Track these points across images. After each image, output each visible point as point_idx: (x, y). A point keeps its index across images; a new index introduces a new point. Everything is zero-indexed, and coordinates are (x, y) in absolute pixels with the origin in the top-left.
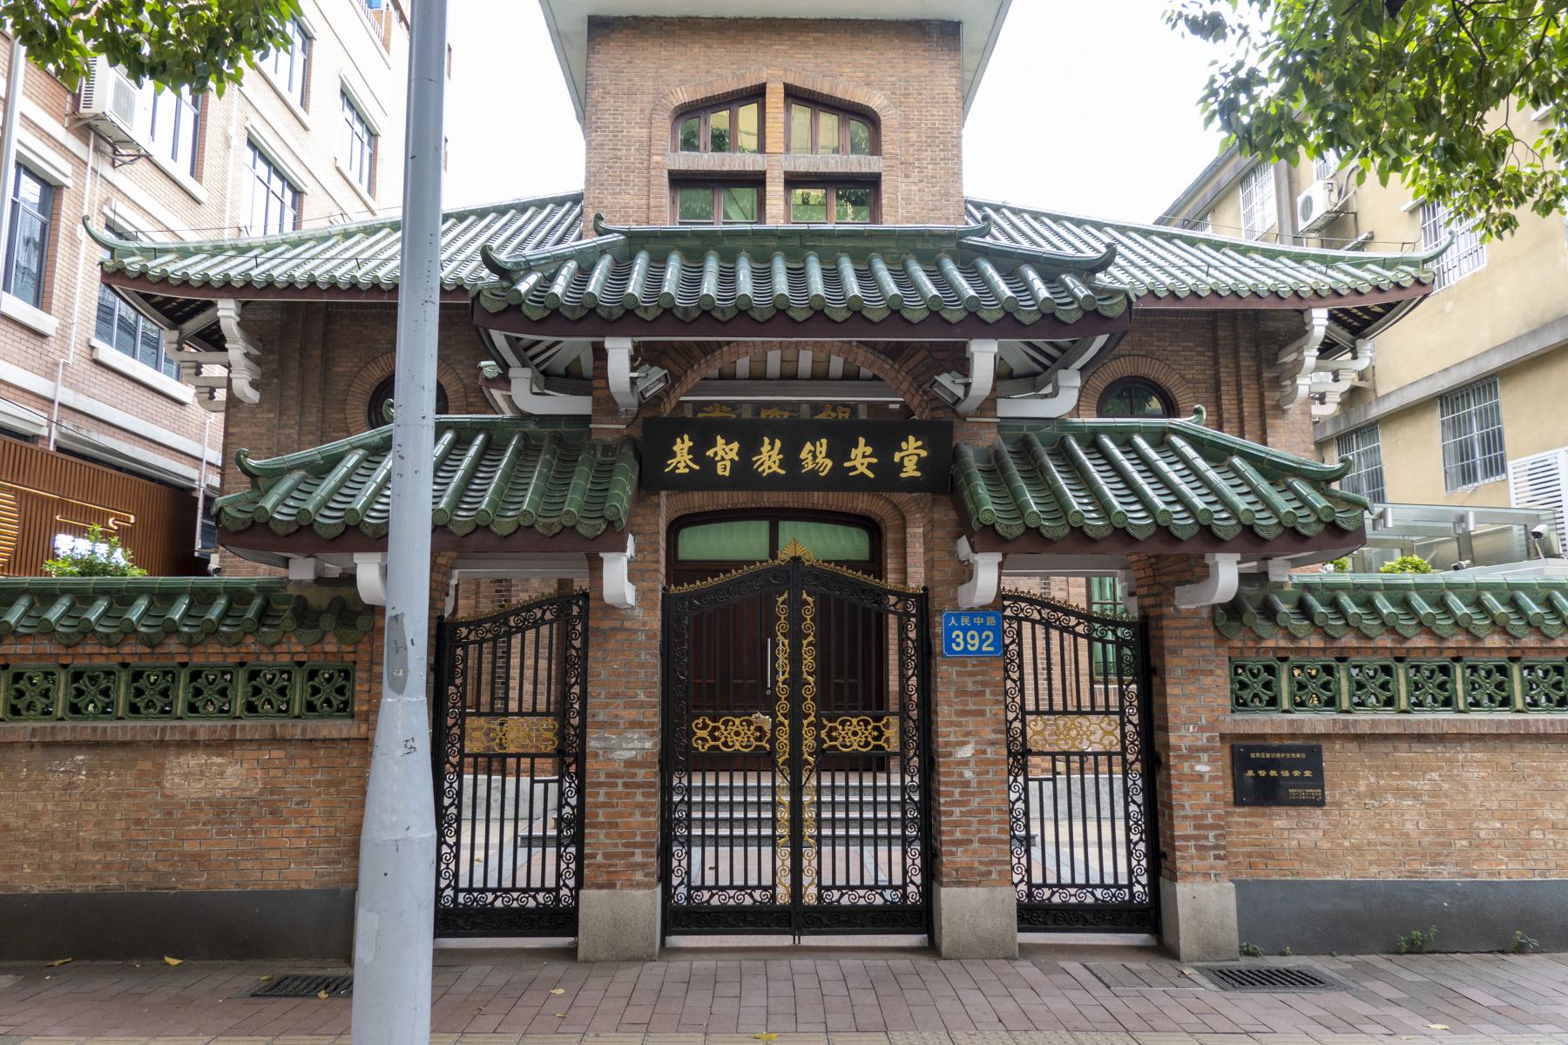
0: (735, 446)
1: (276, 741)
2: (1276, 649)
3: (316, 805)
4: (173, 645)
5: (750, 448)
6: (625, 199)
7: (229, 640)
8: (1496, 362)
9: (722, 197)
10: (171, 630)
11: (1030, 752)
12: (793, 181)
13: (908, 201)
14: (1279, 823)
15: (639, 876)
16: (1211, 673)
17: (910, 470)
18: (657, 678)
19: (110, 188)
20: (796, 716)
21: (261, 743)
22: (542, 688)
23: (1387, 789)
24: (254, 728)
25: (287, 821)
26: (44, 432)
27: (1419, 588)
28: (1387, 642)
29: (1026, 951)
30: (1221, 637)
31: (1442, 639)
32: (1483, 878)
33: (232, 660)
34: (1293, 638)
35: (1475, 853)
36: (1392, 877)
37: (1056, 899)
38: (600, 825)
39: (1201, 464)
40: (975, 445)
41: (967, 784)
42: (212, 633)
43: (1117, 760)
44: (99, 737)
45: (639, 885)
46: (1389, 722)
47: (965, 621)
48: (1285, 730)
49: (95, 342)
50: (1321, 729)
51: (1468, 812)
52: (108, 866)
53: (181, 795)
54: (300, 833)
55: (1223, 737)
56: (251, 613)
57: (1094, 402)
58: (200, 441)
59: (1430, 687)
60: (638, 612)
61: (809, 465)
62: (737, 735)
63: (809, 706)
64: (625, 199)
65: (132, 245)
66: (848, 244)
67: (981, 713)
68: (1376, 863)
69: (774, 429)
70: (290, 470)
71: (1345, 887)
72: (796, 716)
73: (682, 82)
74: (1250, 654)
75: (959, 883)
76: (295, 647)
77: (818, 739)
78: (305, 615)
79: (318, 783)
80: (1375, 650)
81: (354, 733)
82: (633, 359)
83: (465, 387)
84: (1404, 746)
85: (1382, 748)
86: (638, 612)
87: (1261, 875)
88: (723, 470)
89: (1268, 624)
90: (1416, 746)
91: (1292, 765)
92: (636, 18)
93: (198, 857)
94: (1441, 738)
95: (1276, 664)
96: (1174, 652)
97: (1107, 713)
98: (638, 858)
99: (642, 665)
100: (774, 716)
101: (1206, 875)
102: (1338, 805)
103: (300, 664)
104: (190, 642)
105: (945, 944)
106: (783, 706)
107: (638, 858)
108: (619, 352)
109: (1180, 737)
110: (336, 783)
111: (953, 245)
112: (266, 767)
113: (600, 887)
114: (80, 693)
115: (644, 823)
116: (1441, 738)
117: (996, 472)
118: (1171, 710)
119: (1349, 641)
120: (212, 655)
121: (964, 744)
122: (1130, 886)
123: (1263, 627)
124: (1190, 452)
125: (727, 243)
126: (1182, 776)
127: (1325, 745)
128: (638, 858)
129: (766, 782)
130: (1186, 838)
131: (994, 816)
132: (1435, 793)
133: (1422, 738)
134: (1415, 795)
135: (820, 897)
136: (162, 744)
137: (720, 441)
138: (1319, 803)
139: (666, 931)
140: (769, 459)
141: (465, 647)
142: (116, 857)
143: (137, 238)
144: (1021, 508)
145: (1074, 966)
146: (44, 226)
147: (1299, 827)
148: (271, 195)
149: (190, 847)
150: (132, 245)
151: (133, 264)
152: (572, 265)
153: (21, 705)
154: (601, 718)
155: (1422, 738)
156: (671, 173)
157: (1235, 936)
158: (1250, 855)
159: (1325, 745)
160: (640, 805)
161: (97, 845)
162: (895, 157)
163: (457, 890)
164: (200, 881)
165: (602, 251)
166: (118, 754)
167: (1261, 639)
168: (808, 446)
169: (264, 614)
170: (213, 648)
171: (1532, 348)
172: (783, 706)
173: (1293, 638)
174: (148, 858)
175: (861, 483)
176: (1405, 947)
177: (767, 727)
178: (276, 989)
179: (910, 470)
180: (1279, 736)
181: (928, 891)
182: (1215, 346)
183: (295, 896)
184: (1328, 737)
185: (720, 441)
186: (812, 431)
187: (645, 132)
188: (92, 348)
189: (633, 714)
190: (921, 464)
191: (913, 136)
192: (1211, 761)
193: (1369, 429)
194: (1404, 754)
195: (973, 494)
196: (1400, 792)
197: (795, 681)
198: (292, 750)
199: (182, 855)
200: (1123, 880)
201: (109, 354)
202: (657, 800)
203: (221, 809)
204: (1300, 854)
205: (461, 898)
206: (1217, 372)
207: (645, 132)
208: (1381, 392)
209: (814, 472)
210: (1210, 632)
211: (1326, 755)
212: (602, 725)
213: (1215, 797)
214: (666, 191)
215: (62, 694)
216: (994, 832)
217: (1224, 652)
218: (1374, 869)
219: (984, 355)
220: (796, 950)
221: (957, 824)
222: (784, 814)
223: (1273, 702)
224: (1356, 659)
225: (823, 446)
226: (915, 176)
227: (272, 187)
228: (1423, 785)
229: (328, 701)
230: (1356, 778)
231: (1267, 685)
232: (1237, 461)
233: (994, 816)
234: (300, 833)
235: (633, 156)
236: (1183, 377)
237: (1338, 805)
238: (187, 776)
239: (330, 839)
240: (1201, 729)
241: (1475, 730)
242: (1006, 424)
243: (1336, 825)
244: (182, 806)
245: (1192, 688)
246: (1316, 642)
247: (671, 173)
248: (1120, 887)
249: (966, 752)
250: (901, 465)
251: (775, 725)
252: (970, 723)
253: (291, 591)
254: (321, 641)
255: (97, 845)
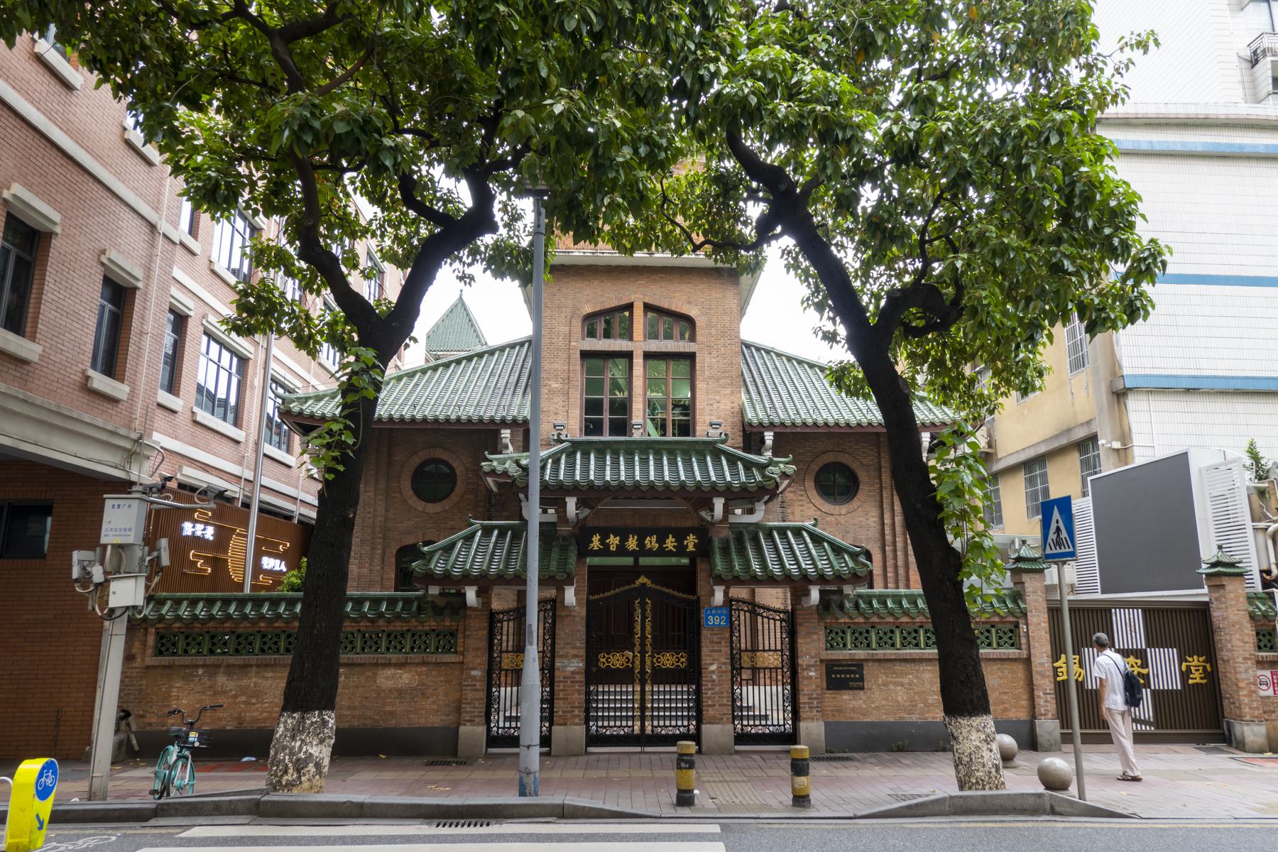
0: (618, 538)
1: (424, 663)
2: (845, 623)
3: (440, 691)
4: (381, 622)
5: (624, 539)
6: (556, 366)
7: (404, 620)
8: (1042, 449)
9: (610, 364)
10: (381, 615)
11: (742, 668)
12: (648, 356)
13: (710, 367)
14: (845, 697)
15: (577, 720)
16: (816, 633)
17: (691, 548)
18: (584, 637)
19: (207, 308)
20: (643, 652)
21: (417, 664)
22: (511, 637)
23: (891, 682)
24: (415, 658)
25: (428, 698)
26: (237, 496)
27: (906, 596)
28: (890, 619)
29: (737, 752)
30: (821, 618)
31: (913, 618)
32: (930, 720)
33: (405, 628)
34: (851, 618)
35: (926, 709)
36: (892, 720)
37: (753, 731)
38: (561, 699)
39: (811, 546)
40: (717, 538)
41: (714, 681)
42: (398, 617)
43: (779, 671)
44: (350, 662)
45: (577, 724)
46: (891, 654)
47: (713, 612)
48: (848, 657)
49: (196, 409)
50: (863, 657)
51: (924, 692)
52: (354, 717)
53: (384, 686)
54: (434, 703)
55: (821, 661)
56: (414, 609)
57: (813, 478)
58: (297, 488)
59: (1005, 639)
60: (577, 608)
61: (649, 546)
62: (617, 661)
63: (649, 648)
64: (556, 366)
65: (293, 396)
66: (666, 447)
67: (720, 651)
68: (886, 714)
69: (635, 531)
70: (435, 551)
71: (872, 723)
72: (643, 652)
73: (588, 301)
74: (835, 625)
75: (710, 723)
76: (432, 624)
77: (653, 663)
78: (438, 611)
79: (441, 681)
80: (887, 623)
81: (457, 660)
82: (577, 504)
83: (466, 468)
84: (898, 664)
85: (889, 665)
86: (577, 608)
87: (837, 719)
88: (613, 548)
89: (840, 613)
90: (903, 664)
91: (850, 672)
92: (562, 265)
93: (392, 713)
94: (913, 661)
95: (846, 629)
96: (801, 625)
97: (776, 650)
98: (576, 712)
99: (578, 631)
100: (633, 652)
101: (813, 719)
102: (870, 689)
103: (434, 630)
104: (389, 621)
105: (704, 749)
106: (637, 648)
107: (576, 712)
108: (571, 503)
109: (803, 661)
110: (448, 681)
111: (711, 448)
112: (419, 674)
113: (561, 725)
114: (239, 644)
115: (578, 698)
116: (913, 661)
117: (725, 551)
118: (799, 650)
119: (875, 619)
120: (398, 626)
121: (712, 664)
122: (784, 725)
123: (839, 614)
124: (808, 540)
125: (615, 446)
126: (804, 678)
127: (865, 664)
128: (576, 713)
129: (630, 689)
130: (805, 703)
131: (725, 695)
132: (910, 684)
133: (905, 660)
134: (902, 685)
135: (652, 731)
136: (376, 665)
137: (612, 536)
138: (862, 688)
139: (587, 746)
140: (632, 544)
141: (502, 623)
142: (356, 713)
143: (295, 392)
144: (732, 567)
145: (756, 757)
146: (176, 342)
147: (854, 699)
148: (236, 232)
149: (388, 708)
150: (293, 396)
151: (295, 407)
152: (550, 461)
153: (163, 649)
154: (561, 653)
155: (905, 660)
156: (581, 351)
157: (824, 744)
158: (832, 711)
159: (865, 664)
160: (577, 690)
161: (349, 708)
162: (703, 343)
163: (498, 728)
164: (392, 723)
165: (562, 451)
166: (357, 669)
167: (838, 619)
168: (648, 538)
169: (420, 609)
170: (398, 624)
171: (1055, 445)
172: (637, 648)
173: (851, 618)
174: (370, 713)
175: (670, 554)
176: (895, 749)
177: (631, 658)
178: (432, 764)
179: (691, 548)
180: (846, 660)
181: (698, 728)
182: (879, 447)
183: (433, 729)
184: (866, 660)
185: (612, 536)
186: (650, 532)
187: (567, 329)
188: (193, 413)
189: (575, 652)
190: (695, 545)
191: (714, 331)
192: (816, 671)
193: (996, 476)
194: (898, 667)
195: (714, 561)
196: (896, 684)
197: (643, 637)
198: (430, 667)
199: (385, 712)
200: (781, 722)
201: (204, 416)
202: (584, 688)
203: (400, 692)
204: (853, 710)
205: (500, 731)
206: (880, 461)
207: (567, 329)
208: (999, 456)
209: (651, 549)
210: (816, 616)
211: (865, 668)
212: (562, 657)
213: (817, 686)
214: (578, 362)
215: (181, 645)
216: (725, 701)
217: (822, 625)
218: (884, 717)
219: (719, 504)
220: (642, 753)
221: (709, 698)
222: (637, 697)
223: (893, 645)
224: (878, 627)
225: (654, 538)
226: (714, 354)
227: (236, 226)
228: (905, 680)
229: (395, 647)
230: (877, 678)
231: (891, 638)
232: (826, 544)
233: (725, 695)
234: (434, 703)
235: (560, 342)
236: (861, 463)
237: (870, 689)
238: (386, 678)
239: (446, 705)
240: (812, 657)
241: (927, 657)
242: (733, 526)
243: (869, 698)
244: (384, 691)
245: (808, 640)
246: (861, 620)
247: (581, 351)
248: (780, 726)
249: (714, 667)
250: (687, 546)
251: (634, 656)
252: (716, 655)
253: (429, 599)
254: (443, 621)
255: (349, 708)
